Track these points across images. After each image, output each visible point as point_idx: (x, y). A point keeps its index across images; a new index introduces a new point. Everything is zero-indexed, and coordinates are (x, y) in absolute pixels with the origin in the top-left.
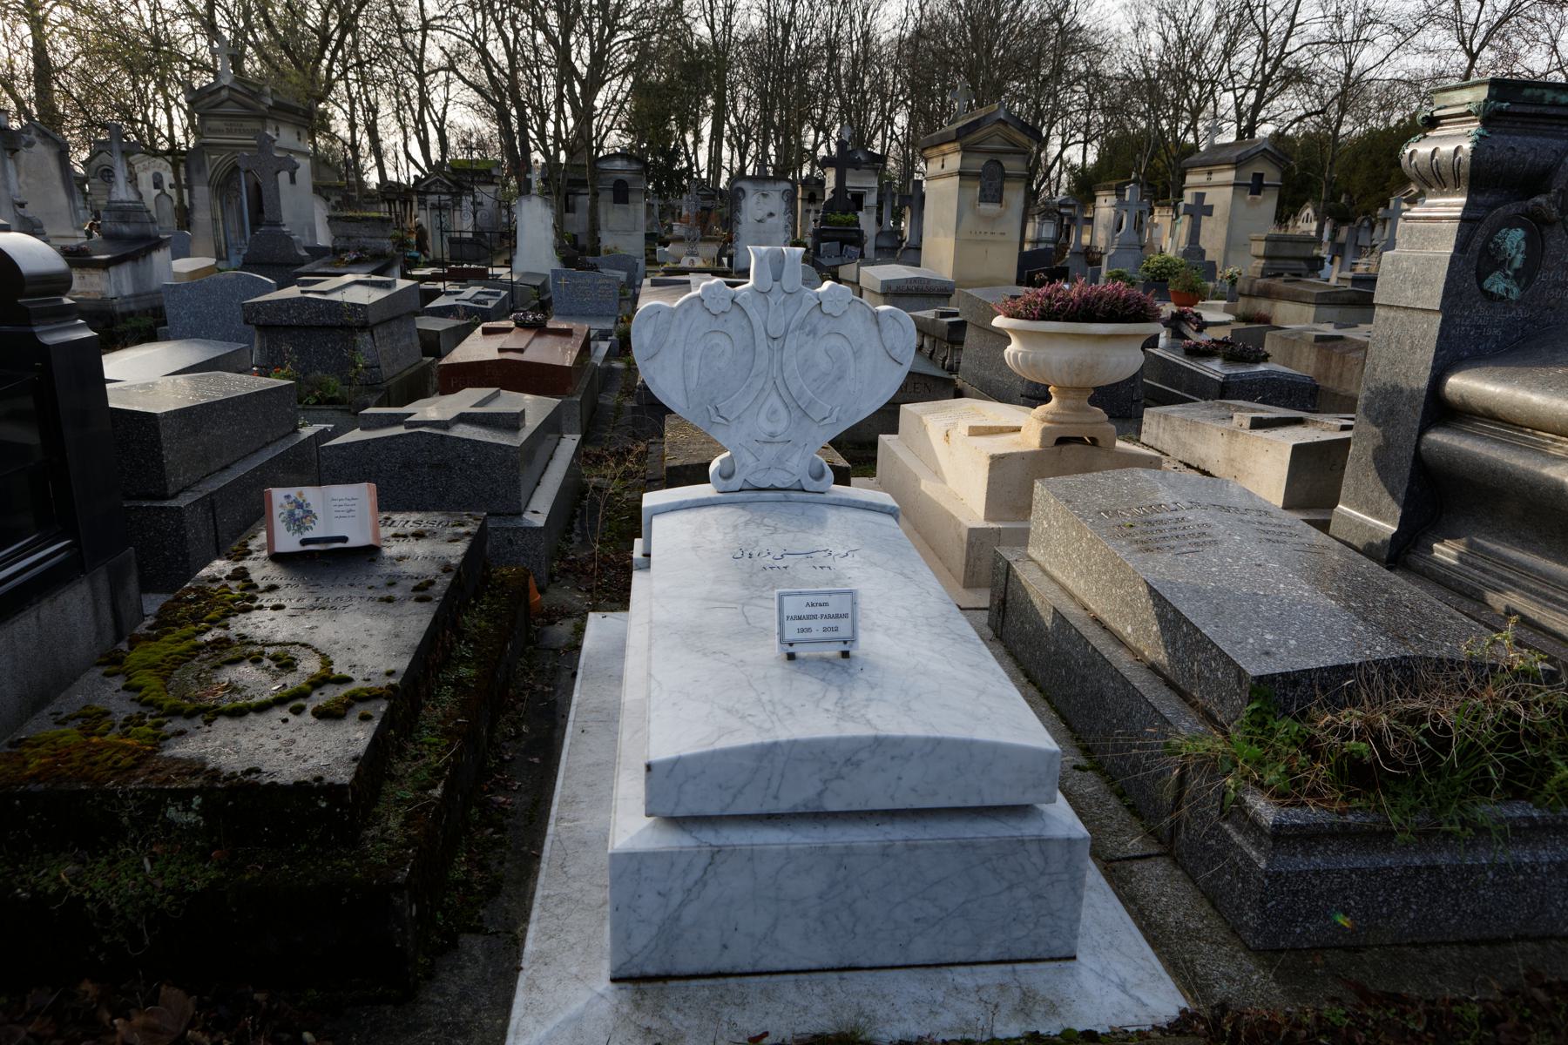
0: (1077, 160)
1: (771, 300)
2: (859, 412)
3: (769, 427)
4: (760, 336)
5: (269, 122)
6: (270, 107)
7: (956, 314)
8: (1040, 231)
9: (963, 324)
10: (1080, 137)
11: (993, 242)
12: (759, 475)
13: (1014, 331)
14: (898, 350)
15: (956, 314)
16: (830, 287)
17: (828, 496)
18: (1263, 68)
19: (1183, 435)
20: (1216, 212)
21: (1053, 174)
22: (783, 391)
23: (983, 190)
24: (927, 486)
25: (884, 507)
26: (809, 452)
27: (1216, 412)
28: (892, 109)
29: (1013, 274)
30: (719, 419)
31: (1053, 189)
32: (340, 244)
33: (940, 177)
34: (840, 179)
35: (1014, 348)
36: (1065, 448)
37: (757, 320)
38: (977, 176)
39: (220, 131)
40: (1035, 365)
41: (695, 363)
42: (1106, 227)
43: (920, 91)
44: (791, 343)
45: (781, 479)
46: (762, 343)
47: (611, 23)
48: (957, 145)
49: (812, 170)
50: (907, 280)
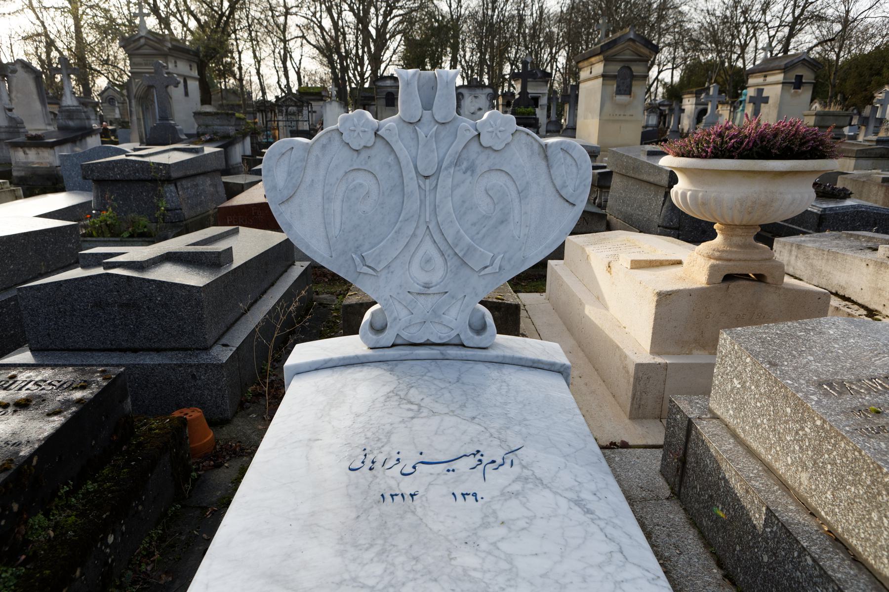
0: (668, 80)
1: (421, 133)
3: (423, 277)
4: (410, 175)
5: (170, 58)
6: (170, 49)
7: (605, 167)
8: (647, 121)
10: (670, 65)
11: (626, 121)
12: (413, 330)
13: (683, 170)
14: (570, 189)
15: (605, 167)
16: (490, 116)
17: (492, 353)
18: (793, 12)
19: (819, 263)
20: (770, 101)
21: (652, 89)
22: (437, 237)
23: (618, 87)
24: (591, 311)
25: (553, 364)
26: (458, 315)
27: (848, 243)
30: (365, 269)
32: (201, 130)
34: (524, 87)
35: (681, 188)
36: (733, 285)
38: (614, 77)
39: (140, 64)
40: (704, 204)
41: (337, 206)
42: (689, 117)
43: (573, 39)
44: (446, 181)
45: (436, 333)
47: (390, 8)
48: (601, 57)
49: (509, 89)
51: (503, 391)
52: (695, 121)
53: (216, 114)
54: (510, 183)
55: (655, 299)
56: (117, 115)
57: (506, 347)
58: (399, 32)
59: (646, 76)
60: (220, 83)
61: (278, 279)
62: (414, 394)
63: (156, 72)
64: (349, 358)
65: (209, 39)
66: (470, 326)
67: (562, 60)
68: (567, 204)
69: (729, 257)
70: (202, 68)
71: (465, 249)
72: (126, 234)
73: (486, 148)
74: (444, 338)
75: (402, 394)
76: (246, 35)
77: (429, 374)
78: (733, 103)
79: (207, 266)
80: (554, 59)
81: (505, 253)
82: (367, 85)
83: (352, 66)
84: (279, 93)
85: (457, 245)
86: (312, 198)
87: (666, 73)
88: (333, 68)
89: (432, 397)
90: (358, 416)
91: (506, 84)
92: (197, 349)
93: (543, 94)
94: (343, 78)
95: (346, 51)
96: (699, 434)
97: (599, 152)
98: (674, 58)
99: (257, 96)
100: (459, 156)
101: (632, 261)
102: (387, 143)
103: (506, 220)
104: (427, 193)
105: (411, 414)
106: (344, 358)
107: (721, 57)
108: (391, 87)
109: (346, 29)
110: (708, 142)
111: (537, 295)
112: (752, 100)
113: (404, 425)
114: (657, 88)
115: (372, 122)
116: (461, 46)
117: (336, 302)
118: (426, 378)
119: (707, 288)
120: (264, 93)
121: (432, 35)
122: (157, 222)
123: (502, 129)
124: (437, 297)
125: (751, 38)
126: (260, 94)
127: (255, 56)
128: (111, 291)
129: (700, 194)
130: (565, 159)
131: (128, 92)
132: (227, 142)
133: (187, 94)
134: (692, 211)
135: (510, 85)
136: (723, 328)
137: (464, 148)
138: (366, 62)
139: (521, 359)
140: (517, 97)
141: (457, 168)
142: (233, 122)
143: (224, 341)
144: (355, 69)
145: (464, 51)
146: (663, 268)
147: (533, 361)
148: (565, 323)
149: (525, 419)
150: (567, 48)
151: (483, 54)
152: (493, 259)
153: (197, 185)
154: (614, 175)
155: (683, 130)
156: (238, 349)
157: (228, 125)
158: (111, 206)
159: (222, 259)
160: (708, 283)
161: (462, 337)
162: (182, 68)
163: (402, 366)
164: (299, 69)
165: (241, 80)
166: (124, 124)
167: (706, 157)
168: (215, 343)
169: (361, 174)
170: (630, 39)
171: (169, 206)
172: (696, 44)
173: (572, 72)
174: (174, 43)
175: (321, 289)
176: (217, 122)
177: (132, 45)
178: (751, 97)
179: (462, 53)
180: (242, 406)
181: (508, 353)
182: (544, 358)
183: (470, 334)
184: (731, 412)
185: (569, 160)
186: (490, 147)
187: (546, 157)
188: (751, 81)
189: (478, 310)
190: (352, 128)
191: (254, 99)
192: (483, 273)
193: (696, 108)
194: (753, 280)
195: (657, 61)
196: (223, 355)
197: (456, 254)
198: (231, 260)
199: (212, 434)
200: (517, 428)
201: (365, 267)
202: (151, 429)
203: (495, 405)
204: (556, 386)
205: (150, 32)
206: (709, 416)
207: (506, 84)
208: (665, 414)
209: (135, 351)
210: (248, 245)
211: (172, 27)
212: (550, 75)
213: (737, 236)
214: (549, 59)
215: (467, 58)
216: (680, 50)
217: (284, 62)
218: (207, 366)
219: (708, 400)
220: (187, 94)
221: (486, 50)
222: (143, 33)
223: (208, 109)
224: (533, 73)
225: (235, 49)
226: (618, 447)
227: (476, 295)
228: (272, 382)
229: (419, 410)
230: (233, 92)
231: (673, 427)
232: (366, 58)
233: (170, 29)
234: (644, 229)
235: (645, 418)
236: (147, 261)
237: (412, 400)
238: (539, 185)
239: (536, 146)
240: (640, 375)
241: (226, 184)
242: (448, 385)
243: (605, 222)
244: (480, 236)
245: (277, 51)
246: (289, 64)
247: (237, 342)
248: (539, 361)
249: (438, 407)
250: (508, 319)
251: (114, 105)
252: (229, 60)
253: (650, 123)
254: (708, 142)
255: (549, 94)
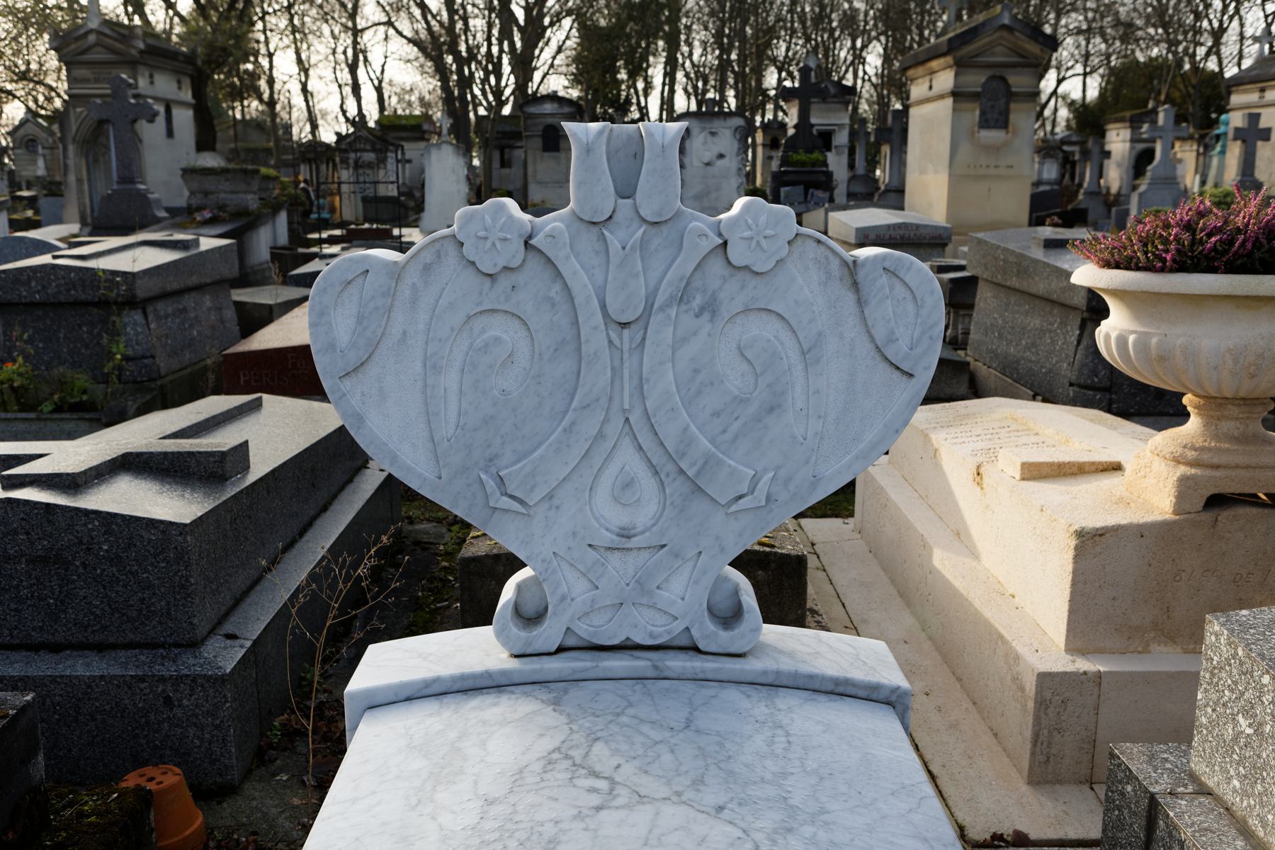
0: (1076, 95)
2: (816, 480)
3: (617, 517)
4: (591, 319)
6: (141, 52)
7: (962, 268)
8: (1040, 172)
9: (973, 280)
10: (1079, 68)
12: (598, 619)
13: (1119, 294)
14: (903, 345)
15: (962, 268)
16: (746, 208)
21: (1047, 112)
22: (645, 439)
23: (983, 113)
24: (944, 562)
25: (876, 687)
26: (694, 581)
28: (864, 47)
29: (1024, 216)
30: (505, 502)
31: (1049, 128)
32: (195, 202)
33: (928, 100)
35: (1116, 330)
36: (1225, 515)
37: (581, 283)
38: (975, 96)
39: (86, 80)
40: (1162, 359)
41: (450, 380)
42: (1119, 165)
44: (661, 332)
46: (595, 337)
48: (949, 60)
49: (775, 116)
50: (889, 226)
51: (779, 747)
52: (1131, 172)
53: (222, 172)
54: (785, 335)
55: (1073, 543)
56: (40, 169)
57: (781, 652)
58: (569, 13)
59: (1037, 93)
60: (233, 108)
61: (334, 497)
62: (601, 756)
63: (114, 95)
64: (474, 676)
65: (214, 31)
66: (710, 609)
67: (874, 59)
68: (898, 373)
69: (1216, 461)
70: (200, 84)
71: (700, 462)
72: (47, 407)
73: (739, 268)
74: (660, 635)
75: (577, 754)
76: (283, 23)
77: (631, 711)
78: (1202, 137)
79: (200, 479)
80: (858, 58)
81: (778, 468)
82: (506, 110)
83: (479, 74)
84: (344, 129)
85: (684, 455)
86: (402, 357)
87: (1072, 83)
88: (444, 79)
89: (637, 763)
90: (490, 802)
91: (770, 106)
92: (177, 645)
93: (841, 126)
94: (462, 97)
95: (469, 49)
96: (1172, 828)
97: (949, 238)
98: (1087, 56)
99: (301, 132)
100: (688, 284)
101: (1023, 465)
102: (549, 260)
103: (780, 406)
104: (626, 356)
105: (595, 800)
106: (463, 677)
107: (1175, 53)
108: (552, 115)
109: (469, 8)
110: (1166, 241)
111: (837, 522)
112: (1240, 134)
113: (583, 825)
114: (1056, 110)
115: (520, 221)
116: (683, 37)
117: (447, 538)
118: (624, 719)
119: (1175, 522)
120: (314, 127)
121: (630, 18)
122: (106, 382)
123: (769, 232)
124: (645, 555)
125: (1231, 18)
126: (308, 128)
127: (299, 61)
128: (16, 532)
129: (1154, 340)
130: (892, 288)
131: (62, 128)
132: (242, 226)
133: (170, 133)
134: (1137, 371)
135: (777, 108)
136: (1214, 610)
137: (695, 269)
138: (506, 68)
139: (811, 677)
140: (791, 132)
141: (684, 307)
142: (255, 185)
143: (228, 628)
144: (485, 81)
145: (690, 45)
146: (1085, 478)
147: (836, 681)
148: (893, 581)
149: (823, 811)
150: (883, 38)
151: (725, 50)
152: (755, 481)
153: (185, 310)
154: (981, 284)
155: (1108, 189)
156: (255, 642)
157: (246, 192)
158: (22, 352)
159: (228, 466)
160: (1176, 512)
161: (694, 632)
162: (164, 85)
163: (577, 694)
164: (380, 82)
165: (272, 103)
166: (53, 188)
167: (1162, 270)
168: (212, 632)
169: (498, 320)
170: (1004, 27)
171: (130, 353)
172: (1127, 31)
173: (894, 83)
174: (150, 41)
175: (417, 513)
176: (225, 186)
177: (73, 46)
178: (1237, 129)
179: (685, 49)
180: (261, 758)
181: (786, 665)
182: (858, 674)
183: (711, 626)
184: (1236, 783)
185: (900, 290)
186: (746, 268)
187: (855, 285)
188: (1235, 99)
189: (726, 579)
190: (481, 234)
191: (295, 138)
192: (734, 508)
193: (1132, 148)
194: (1262, 505)
195: (1054, 63)
196: (226, 657)
197: (682, 472)
198: (246, 468)
199: (200, 820)
200: (808, 830)
201: (505, 499)
202: (81, 815)
203: (763, 780)
204: (882, 734)
205: (109, 23)
206: (1190, 789)
207: (770, 106)
208: (1101, 773)
209: (56, 648)
210: (276, 433)
211: (147, 10)
212: (852, 90)
213: (1228, 418)
214: (850, 58)
215: (695, 58)
216: (1098, 40)
217: (353, 68)
218: (194, 680)
219: (1186, 754)
220: (170, 133)
221: (731, 45)
222: (94, 24)
223: (210, 160)
224: (819, 87)
225: (263, 50)
226: (1008, 844)
227: (722, 550)
228: (320, 706)
229: (612, 790)
230: (256, 125)
231: (1119, 808)
232: (505, 60)
233: (143, 16)
234: (1045, 394)
235: (1058, 780)
236: (85, 472)
237: (598, 768)
238: (841, 337)
239: (835, 264)
240: (1048, 695)
241: (239, 305)
242: (667, 734)
243: (966, 378)
244: (727, 436)
245: (340, 49)
246: (361, 72)
247: (255, 630)
248: (848, 682)
249: (651, 786)
250: (782, 584)
251: (35, 152)
252: (250, 66)
253: (1045, 176)
254: (1166, 241)
255: (851, 126)
